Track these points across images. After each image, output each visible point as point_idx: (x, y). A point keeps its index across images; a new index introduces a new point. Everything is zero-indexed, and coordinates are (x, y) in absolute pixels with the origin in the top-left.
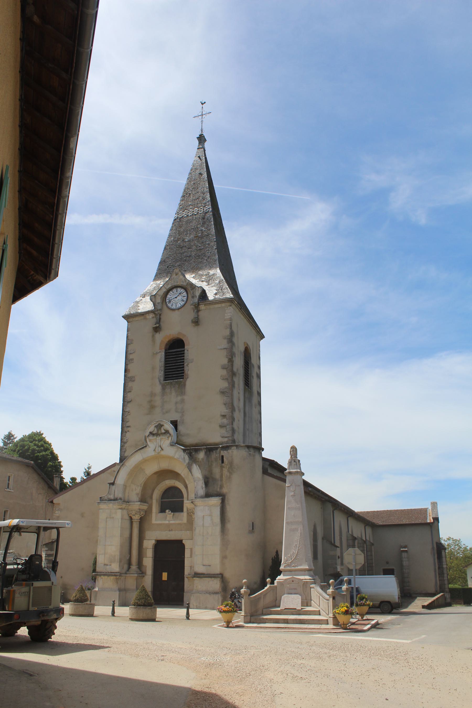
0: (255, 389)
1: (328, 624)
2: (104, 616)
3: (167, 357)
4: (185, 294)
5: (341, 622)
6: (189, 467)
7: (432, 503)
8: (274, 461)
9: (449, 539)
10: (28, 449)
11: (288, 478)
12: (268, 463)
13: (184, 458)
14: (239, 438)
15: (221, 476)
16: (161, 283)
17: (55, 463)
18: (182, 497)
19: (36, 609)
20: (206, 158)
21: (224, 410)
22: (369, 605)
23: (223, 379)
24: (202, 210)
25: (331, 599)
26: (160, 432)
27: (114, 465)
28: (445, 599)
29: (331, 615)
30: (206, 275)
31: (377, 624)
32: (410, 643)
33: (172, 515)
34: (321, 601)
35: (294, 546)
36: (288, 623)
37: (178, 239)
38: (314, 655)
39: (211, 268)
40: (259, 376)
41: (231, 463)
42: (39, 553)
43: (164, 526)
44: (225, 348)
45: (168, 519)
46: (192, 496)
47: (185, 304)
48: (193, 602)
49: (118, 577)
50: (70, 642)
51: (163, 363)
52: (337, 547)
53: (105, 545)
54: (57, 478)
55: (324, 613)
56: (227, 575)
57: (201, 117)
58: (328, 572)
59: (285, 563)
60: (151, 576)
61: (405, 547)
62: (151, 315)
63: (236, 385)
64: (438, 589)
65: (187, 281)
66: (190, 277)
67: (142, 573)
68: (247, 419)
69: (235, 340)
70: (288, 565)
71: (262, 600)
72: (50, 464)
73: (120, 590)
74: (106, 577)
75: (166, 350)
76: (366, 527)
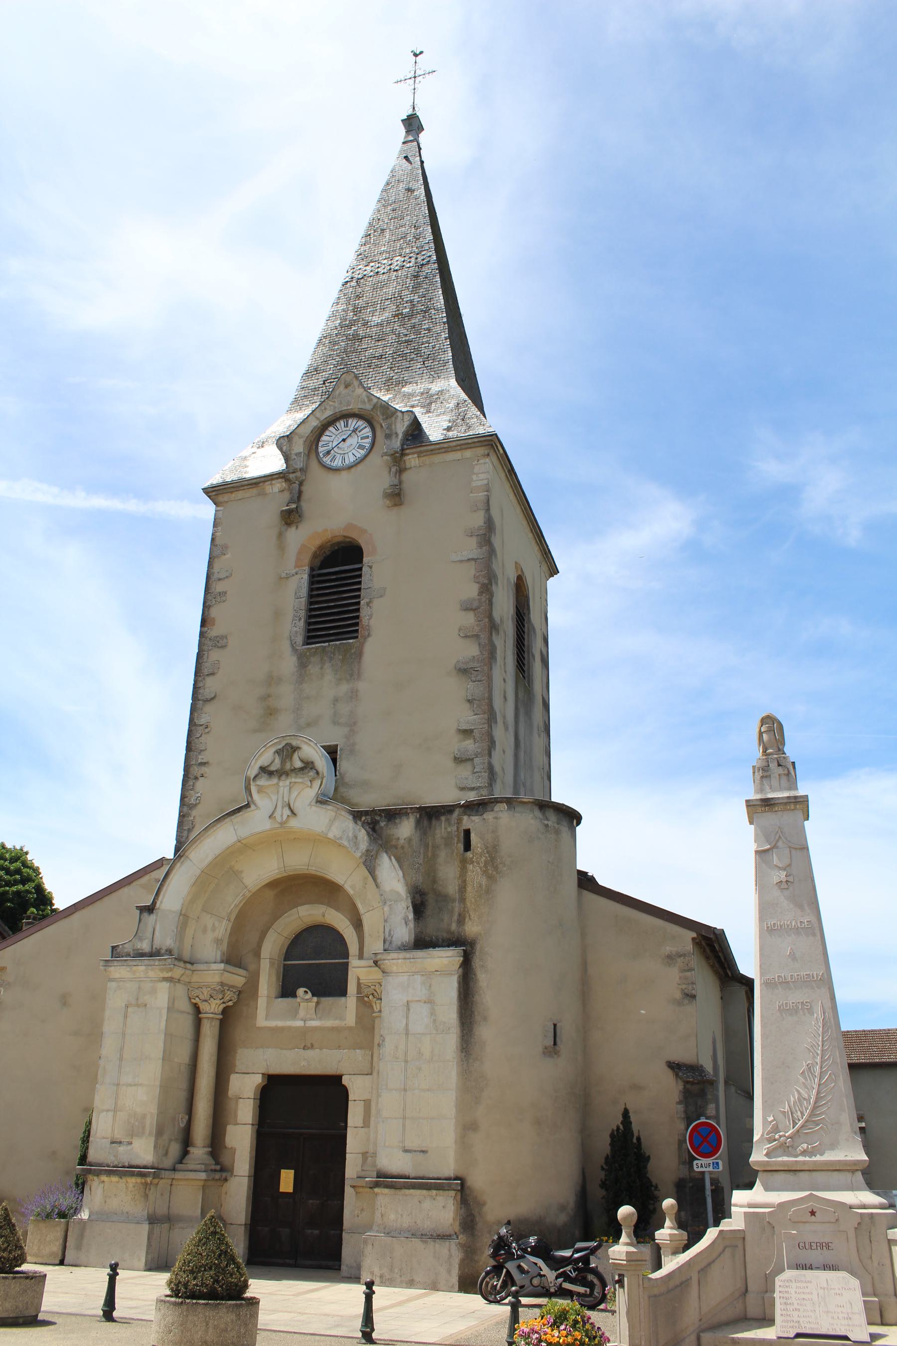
3: (316, 579)
4: (367, 431)
6: (370, 864)
15: (463, 889)
17: (43, 911)
18: (346, 955)
21: (468, 717)
23: (466, 636)
24: (413, 260)
26: (288, 766)
27: (161, 862)
30: (422, 394)
41: (492, 851)
43: (289, 1036)
44: (472, 559)
45: (302, 1013)
47: (366, 456)
49: (149, 1180)
51: (304, 601)
53: (118, 1085)
56: (478, 1181)
57: (412, 81)
59: (770, 1140)
62: (279, 485)
65: (375, 400)
67: (222, 1170)
69: (496, 541)
70: (784, 1148)
72: (33, 913)
73: (153, 1220)
74: (115, 1179)
75: (312, 569)
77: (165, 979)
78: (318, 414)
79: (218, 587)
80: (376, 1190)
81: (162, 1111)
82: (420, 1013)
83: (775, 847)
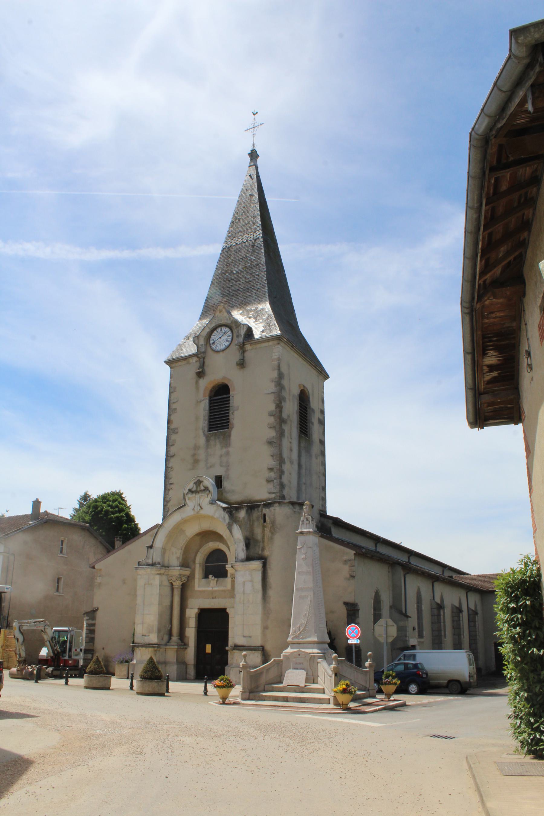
0: (315, 437)
1: (330, 703)
3: (212, 402)
4: (230, 333)
8: (338, 518)
10: (102, 510)
12: (331, 521)
13: (224, 517)
14: (291, 494)
15: (263, 537)
16: (206, 321)
18: (226, 561)
22: (395, 684)
23: (271, 428)
25: (333, 676)
26: (199, 489)
30: (254, 310)
33: (215, 581)
36: (287, 701)
37: (226, 272)
39: (260, 302)
40: (322, 422)
41: (273, 523)
43: (206, 593)
45: (211, 585)
47: (229, 345)
49: (156, 649)
51: (207, 412)
53: (143, 614)
54: (118, 542)
57: (252, 130)
62: (195, 359)
63: (287, 434)
65: (232, 319)
66: (237, 315)
68: (303, 471)
69: (285, 382)
70: (296, 637)
71: (264, 674)
74: (144, 649)
75: (210, 397)
76: (469, 594)
77: (158, 574)
78: (209, 326)
79: (174, 406)
81: (160, 623)
82: (249, 586)
83: (303, 547)
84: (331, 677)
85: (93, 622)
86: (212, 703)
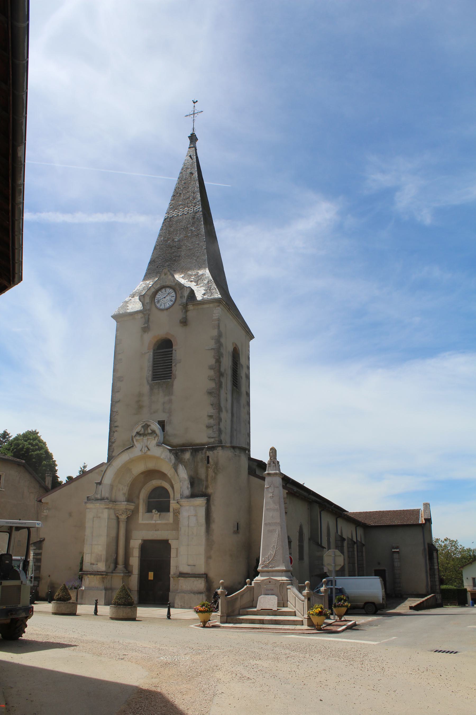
0: (243, 389)
2: (86, 615)
4: (173, 294)
5: (315, 623)
7: (424, 504)
8: (262, 461)
9: (446, 540)
10: (23, 448)
11: (268, 479)
12: (256, 464)
13: (170, 458)
14: (226, 438)
16: (150, 283)
18: (169, 497)
19: (5, 607)
20: (197, 157)
21: (211, 411)
22: (347, 606)
23: (210, 380)
25: (306, 600)
26: (146, 432)
27: (103, 464)
28: (436, 599)
29: (306, 616)
30: (195, 275)
31: (355, 625)
32: (378, 644)
34: (297, 601)
35: (272, 545)
36: (263, 623)
37: (168, 239)
38: (273, 655)
39: (200, 268)
40: (248, 377)
41: (216, 464)
42: (10, 553)
43: (149, 527)
45: (154, 518)
46: (178, 496)
47: (173, 305)
48: (178, 601)
49: (104, 576)
50: (40, 640)
51: (151, 363)
52: (324, 548)
54: (49, 477)
55: (300, 614)
56: (212, 575)
57: (192, 116)
58: (308, 572)
59: (263, 564)
60: (137, 576)
61: (397, 548)
64: (429, 590)
65: (176, 281)
66: (179, 278)
70: (266, 566)
72: (44, 463)
73: (106, 589)
74: (92, 576)
75: (154, 350)
76: (357, 528)
77: (106, 508)
78: (154, 286)
80: (179, 578)
81: (107, 553)
83: (270, 486)
84: (303, 601)
85: (40, 551)
86: (192, 626)
